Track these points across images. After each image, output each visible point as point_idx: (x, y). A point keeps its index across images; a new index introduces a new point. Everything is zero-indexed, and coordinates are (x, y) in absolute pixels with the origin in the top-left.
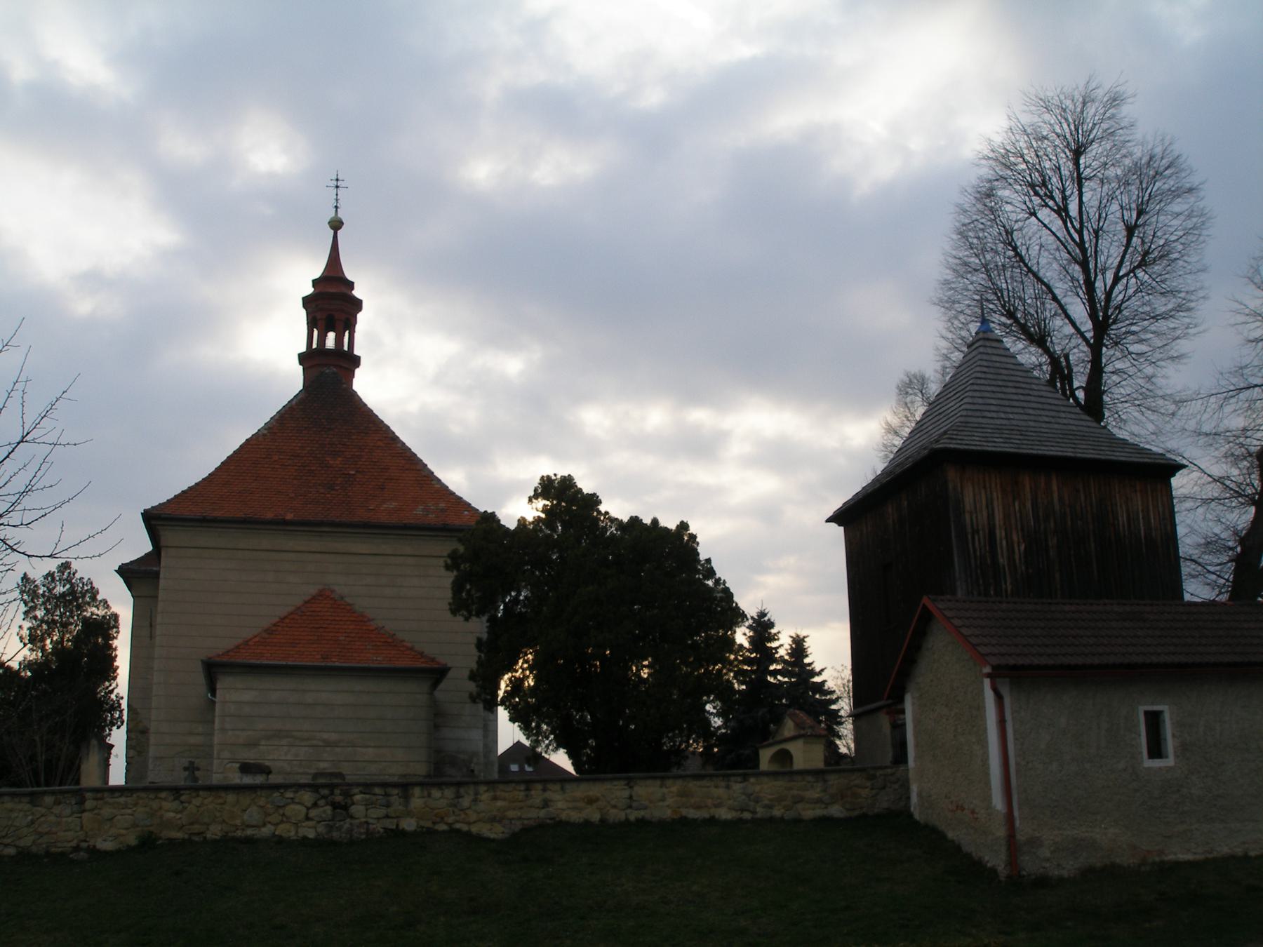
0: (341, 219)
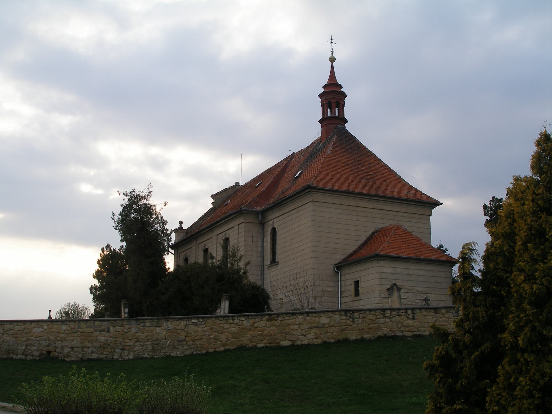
0: (334, 57)
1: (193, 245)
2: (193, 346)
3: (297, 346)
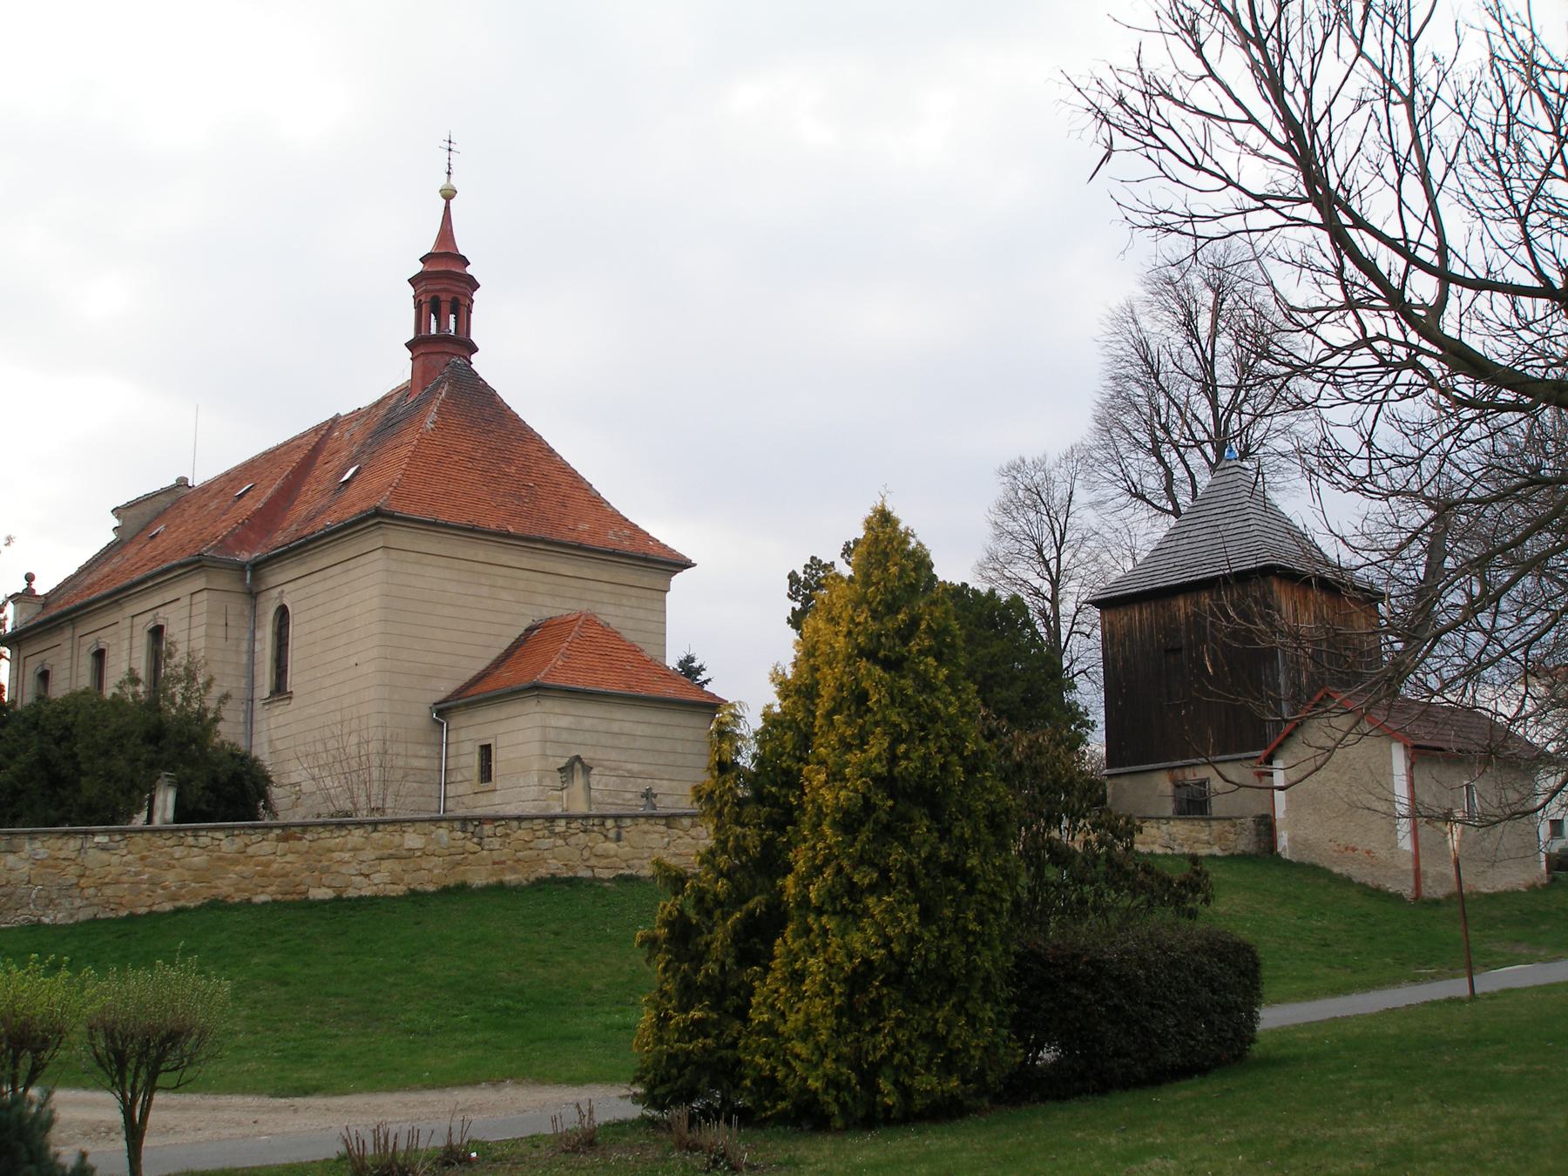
1: (65, 638)
2: (96, 900)
3: (349, 899)
